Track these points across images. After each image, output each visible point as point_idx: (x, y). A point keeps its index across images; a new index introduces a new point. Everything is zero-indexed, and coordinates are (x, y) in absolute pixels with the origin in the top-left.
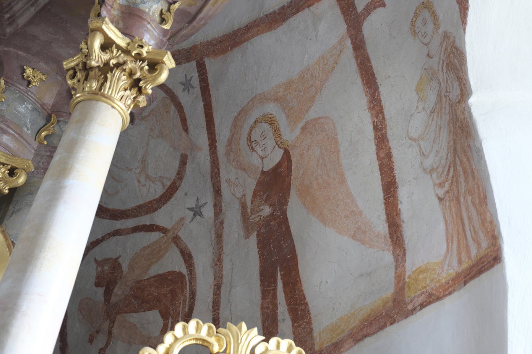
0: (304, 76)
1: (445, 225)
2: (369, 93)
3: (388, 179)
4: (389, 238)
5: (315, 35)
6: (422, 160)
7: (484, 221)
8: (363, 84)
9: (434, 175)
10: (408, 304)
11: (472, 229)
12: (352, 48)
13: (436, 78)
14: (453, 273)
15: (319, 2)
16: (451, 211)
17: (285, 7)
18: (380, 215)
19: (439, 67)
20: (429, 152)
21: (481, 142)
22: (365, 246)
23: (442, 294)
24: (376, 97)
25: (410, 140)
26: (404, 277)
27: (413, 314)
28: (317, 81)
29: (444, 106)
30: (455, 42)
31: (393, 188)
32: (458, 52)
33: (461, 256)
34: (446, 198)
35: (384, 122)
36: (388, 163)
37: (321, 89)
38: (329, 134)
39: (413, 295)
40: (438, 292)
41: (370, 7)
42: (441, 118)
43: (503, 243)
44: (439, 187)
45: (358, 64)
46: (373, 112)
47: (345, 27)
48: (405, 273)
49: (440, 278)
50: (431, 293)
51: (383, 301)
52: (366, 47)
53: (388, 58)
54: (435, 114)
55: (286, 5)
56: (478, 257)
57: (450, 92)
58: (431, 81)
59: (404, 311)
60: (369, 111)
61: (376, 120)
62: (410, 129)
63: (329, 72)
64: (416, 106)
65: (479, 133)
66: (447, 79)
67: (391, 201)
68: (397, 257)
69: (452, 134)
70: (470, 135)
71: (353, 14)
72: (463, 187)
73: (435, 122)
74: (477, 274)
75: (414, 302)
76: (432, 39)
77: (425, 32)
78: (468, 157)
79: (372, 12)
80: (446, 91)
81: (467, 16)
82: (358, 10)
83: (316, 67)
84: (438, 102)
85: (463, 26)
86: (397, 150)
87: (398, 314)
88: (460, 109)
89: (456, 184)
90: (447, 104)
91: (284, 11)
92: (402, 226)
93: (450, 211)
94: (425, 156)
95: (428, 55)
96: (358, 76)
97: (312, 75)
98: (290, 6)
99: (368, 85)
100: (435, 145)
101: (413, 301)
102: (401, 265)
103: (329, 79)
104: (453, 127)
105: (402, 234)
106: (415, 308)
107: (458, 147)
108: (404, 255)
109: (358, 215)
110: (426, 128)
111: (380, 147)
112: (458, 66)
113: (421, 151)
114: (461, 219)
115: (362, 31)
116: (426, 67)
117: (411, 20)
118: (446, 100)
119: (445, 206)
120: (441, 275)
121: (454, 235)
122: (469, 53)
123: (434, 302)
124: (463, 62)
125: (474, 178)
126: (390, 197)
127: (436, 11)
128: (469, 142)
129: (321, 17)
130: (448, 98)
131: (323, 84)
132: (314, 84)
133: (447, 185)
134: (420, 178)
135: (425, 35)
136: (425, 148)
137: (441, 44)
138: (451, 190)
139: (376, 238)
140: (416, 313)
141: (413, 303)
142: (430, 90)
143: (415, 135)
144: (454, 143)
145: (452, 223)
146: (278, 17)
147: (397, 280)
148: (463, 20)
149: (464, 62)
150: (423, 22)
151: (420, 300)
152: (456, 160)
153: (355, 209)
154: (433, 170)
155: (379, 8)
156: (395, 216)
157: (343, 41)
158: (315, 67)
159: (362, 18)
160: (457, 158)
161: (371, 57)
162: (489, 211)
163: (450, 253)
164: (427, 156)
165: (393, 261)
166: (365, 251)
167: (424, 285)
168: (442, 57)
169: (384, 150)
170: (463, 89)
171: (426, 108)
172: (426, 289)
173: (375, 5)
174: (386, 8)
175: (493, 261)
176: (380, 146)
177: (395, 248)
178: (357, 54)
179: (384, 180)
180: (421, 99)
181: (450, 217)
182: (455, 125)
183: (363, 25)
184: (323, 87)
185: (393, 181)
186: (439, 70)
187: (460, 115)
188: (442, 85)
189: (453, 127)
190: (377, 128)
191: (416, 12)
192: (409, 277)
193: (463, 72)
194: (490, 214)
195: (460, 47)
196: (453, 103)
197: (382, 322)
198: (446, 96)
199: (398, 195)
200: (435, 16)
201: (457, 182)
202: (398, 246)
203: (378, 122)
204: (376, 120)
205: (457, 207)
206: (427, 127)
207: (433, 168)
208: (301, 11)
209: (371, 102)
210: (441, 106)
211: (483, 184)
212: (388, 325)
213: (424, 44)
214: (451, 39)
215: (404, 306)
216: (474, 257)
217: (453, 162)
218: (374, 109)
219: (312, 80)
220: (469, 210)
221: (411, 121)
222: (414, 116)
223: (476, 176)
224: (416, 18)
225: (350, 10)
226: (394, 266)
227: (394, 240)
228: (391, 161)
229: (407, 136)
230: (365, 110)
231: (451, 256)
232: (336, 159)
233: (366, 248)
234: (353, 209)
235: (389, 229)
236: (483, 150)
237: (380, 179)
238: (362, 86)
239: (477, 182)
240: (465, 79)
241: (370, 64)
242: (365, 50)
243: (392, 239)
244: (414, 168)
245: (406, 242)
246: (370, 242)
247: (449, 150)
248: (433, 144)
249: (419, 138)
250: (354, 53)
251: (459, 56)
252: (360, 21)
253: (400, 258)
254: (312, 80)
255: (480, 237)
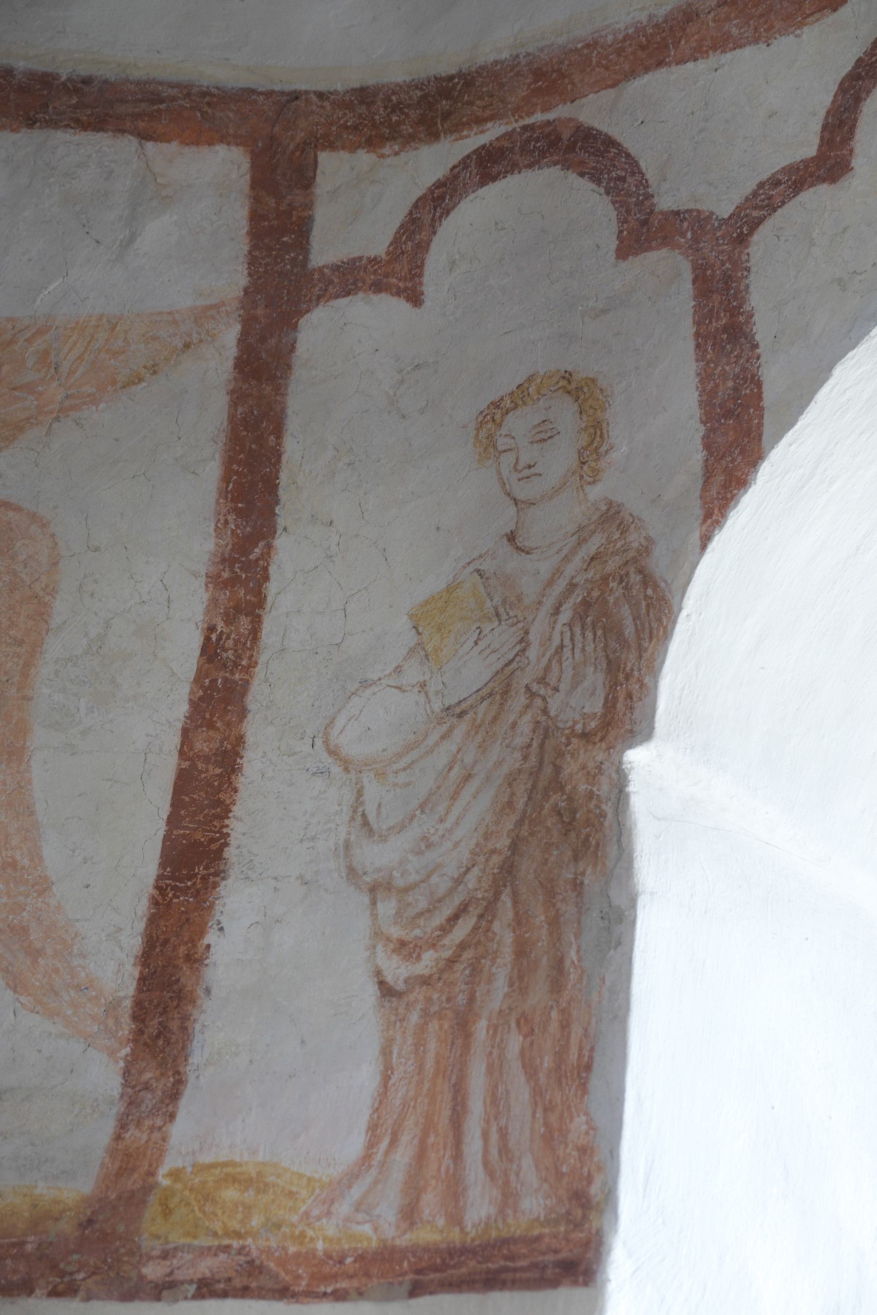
0: (12, 342)
1: (378, 1078)
2: (233, 531)
3: (195, 829)
4: (127, 1015)
5: (122, 237)
6: (353, 838)
7: (556, 1134)
8: (223, 493)
9: (387, 908)
10: (145, 1258)
11: (494, 1137)
12: (235, 358)
13: (518, 622)
14: (371, 1239)
15: (187, 144)
16: (419, 1044)
17: (56, 82)
18: (120, 930)
19: (543, 596)
20: (393, 827)
21: (636, 895)
22: (17, 999)
23: (304, 1283)
24: (252, 557)
25: (325, 755)
26: (150, 1165)
27: (158, 1298)
28: (55, 384)
29: (512, 718)
30: (648, 555)
31: (207, 868)
32: (650, 592)
33: (418, 1199)
34: (412, 997)
35: (252, 649)
36: (216, 784)
37: (57, 419)
38: (23, 576)
39: (176, 1238)
40: (287, 1272)
41: (361, 273)
42: (483, 748)
43: (616, 1231)
44: (394, 951)
45: (232, 418)
46: (223, 597)
47: (242, 280)
48: (161, 1155)
49: (310, 1233)
50: (257, 1262)
51: (35, 1206)
52: (286, 386)
53: (349, 464)
54: (462, 728)
55: (63, 79)
56: (494, 1234)
57: (556, 689)
58: (490, 620)
59: (122, 1274)
60: (206, 585)
61: (220, 626)
62: (340, 722)
63: (114, 382)
64: (394, 665)
65: (636, 866)
66: (562, 646)
67: (181, 904)
68: (139, 1091)
69: (514, 818)
70: (596, 857)
71: (288, 259)
72: (500, 995)
73: (454, 748)
74: (474, 1282)
75: (175, 1262)
76: (551, 498)
77: (532, 464)
78: (557, 917)
79: (361, 295)
80: (542, 680)
81: (733, 503)
82: (311, 257)
83: (74, 338)
84: (491, 694)
85: (704, 528)
86: (264, 760)
87: (93, 1273)
88: (580, 761)
89: (467, 972)
90: (527, 717)
91: (45, 92)
92: (199, 1002)
93: (417, 1046)
94: (371, 830)
95: (511, 538)
96: (213, 456)
97: (46, 353)
98: (77, 90)
99: (240, 505)
100: (423, 816)
101: (174, 1257)
102: (148, 1123)
103: (102, 406)
104: (530, 798)
105: (190, 1031)
106: (173, 1281)
107: (527, 869)
108: (174, 1095)
109: (33, 887)
110: (409, 748)
111: (204, 718)
112: (629, 631)
113: (361, 809)
114: (454, 1085)
115: (295, 327)
116: (486, 566)
117: (494, 397)
118: (527, 707)
119: (402, 1021)
120: (318, 1224)
121: (410, 1123)
122: (688, 615)
123: (263, 1298)
124: (658, 629)
125: (557, 984)
126: (185, 891)
127: (608, 424)
128: (583, 874)
129: (171, 197)
130: (538, 702)
131: (73, 408)
132: (40, 388)
133: (428, 961)
134: (326, 890)
135: (527, 472)
136: (379, 805)
137: (582, 535)
138: (441, 981)
139: (72, 993)
140: (176, 1300)
141: (168, 1263)
142: (476, 643)
143: (353, 750)
144: (514, 847)
145: (410, 1083)
146: (11, 97)
147: (117, 1164)
148: (713, 509)
149: (661, 632)
150: (539, 429)
151: (205, 1267)
152: (499, 904)
153: (26, 862)
154: (389, 890)
155: (392, 295)
156: (181, 960)
157: (213, 318)
158: (70, 337)
159: (316, 291)
160: (506, 899)
161: (293, 424)
162: (586, 1114)
163: (373, 1172)
164: (380, 836)
165: (118, 1097)
166: (12, 1015)
167: (235, 1225)
168: (570, 570)
169: (218, 737)
170: (620, 706)
171: (432, 688)
172: (241, 1242)
173: (385, 280)
174: (418, 310)
175: (557, 1270)
176: (208, 716)
177: (142, 1060)
178: (244, 387)
179: (178, 828)
180: (423, 653)
181: (410, 1062)
182: (539, 796)
183: (308, 312)
184: (68, 416)
185: (214, 847)
186: (540, 603)
187: (575, 777)
188: (533, 653)
189: (526, 799)
190: (217, 655)
191: (526, 385)
192: (176, 1174)
193: (640, 657)
194: (587, 1123)
195: (666, 582)
196: (558, 728)
197: (15, 1271)
198: (531, 694)
199: (216, 899)
200: (598, 439)
201: (473, 970)
202: (156, 1058)
203: (228, 638)
204: (220, 626)
205: (453, 1044)
206: (412, 749)
207: (389, 883)
208: (110, 133)
209: (226, 561)
210: (499, 714)
211: (589, 1023)
212: (38, 1292)
213: (509, 495)
214: (634, 539)
215: (126, 1259)
216: (474, 1225)
217: (484, 903)
218: (231, 592)
219: (39, 371)
220: (501, 1073)
221: (356, 699)
222: (374, 688)
223: (569, 987)
224: (516, 407)
225: (285, 239)
226: (114, 1111)
227: (146, 1031)
228: (231, 783)
229: (321, 735)
230: (196, 575)
231: (376, 1182)
232: (20, 667)
233: (18, 1005)
234: (18, 858)
235: (139, 990)
236: (634, 922)
237: (165, 817)
238: (214, 495)
239: (564, 1005)
240: (640, 681)
241: (279, 444)
242: (280, 390)
243: (142, 1025)
244: (313, 848)
245: (195, 1059)
246: (44, 995)
247: (482, 859)
248: (418, 812)
249: (366, 765)
250: (235, 379)
251: (648, 606)
252: (306, 296)
253: (149, 1100)
254: (39, 371)
255: (521, 1175)
